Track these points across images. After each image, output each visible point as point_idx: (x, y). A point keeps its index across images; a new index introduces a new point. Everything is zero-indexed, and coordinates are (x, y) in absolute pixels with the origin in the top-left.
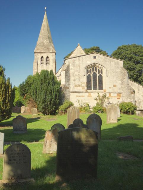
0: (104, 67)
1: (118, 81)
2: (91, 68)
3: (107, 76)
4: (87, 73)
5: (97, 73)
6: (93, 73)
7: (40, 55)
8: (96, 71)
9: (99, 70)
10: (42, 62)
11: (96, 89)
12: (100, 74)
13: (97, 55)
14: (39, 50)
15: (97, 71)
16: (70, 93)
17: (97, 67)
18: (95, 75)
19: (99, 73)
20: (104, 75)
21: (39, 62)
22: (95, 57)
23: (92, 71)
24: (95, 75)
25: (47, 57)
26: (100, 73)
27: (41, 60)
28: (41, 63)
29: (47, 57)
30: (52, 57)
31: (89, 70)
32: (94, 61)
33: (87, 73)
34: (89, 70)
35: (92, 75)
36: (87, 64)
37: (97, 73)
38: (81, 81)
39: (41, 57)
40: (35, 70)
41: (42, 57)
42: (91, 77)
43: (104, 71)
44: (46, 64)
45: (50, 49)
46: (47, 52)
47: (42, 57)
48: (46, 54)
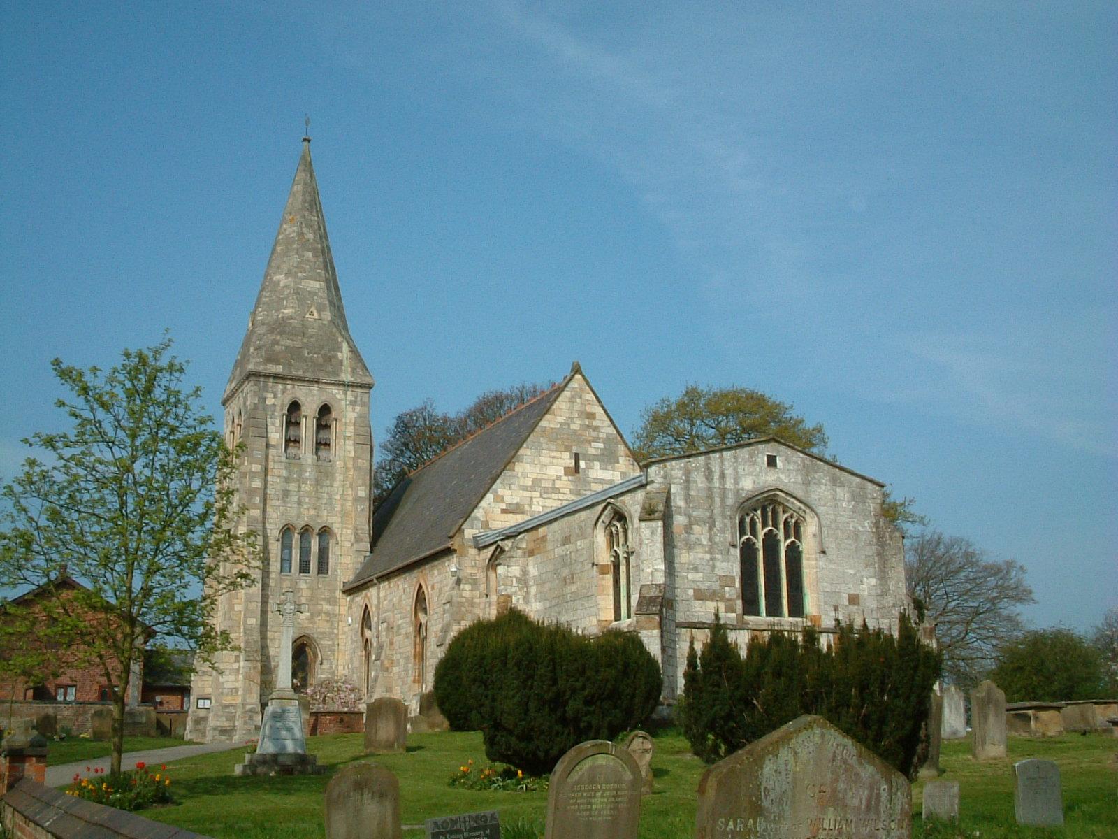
0: (808, 511)
1: (865, 579)
2: (756, 510)
3: (824, 552)
4: (742, 533)
5: (781, 536)
6: (765, 534)
7: (284, 391)
8: (775, 525)
9: (786, 522)
10: (323, 435)
11: (756, 613)
12: (748, 539)
13: (784, 457)
14: (277, 362)
15: (781, 526)
16: (678, 631)
17: (780, 510)
18: (771, 543)
19: (787, 537)
20: (808, 546)
21: (276, 435)
22: (772, 461)
23: (759, 526)
24: (771, 543)
25: (325, 410)
26: (793, 539)
27: (289, 424)
28: (288, 441)
29: (325, 410)
30: (350, 408)
31: (748, 519)
32: (770, 479)
33: (786, 539)
34: (748, 519)
35: (759, 545)
36: (742, 489)
37: (781, 536)
38: (719, 572)
39: (287, 403)
40: (254, 475)
41: (295, 406)
42: (755, 551)
43: (810, 527)
44: (317, 449)
45: (341, 362)
46: (323, 378)
47: (295, 406)
48: (315, 389)
